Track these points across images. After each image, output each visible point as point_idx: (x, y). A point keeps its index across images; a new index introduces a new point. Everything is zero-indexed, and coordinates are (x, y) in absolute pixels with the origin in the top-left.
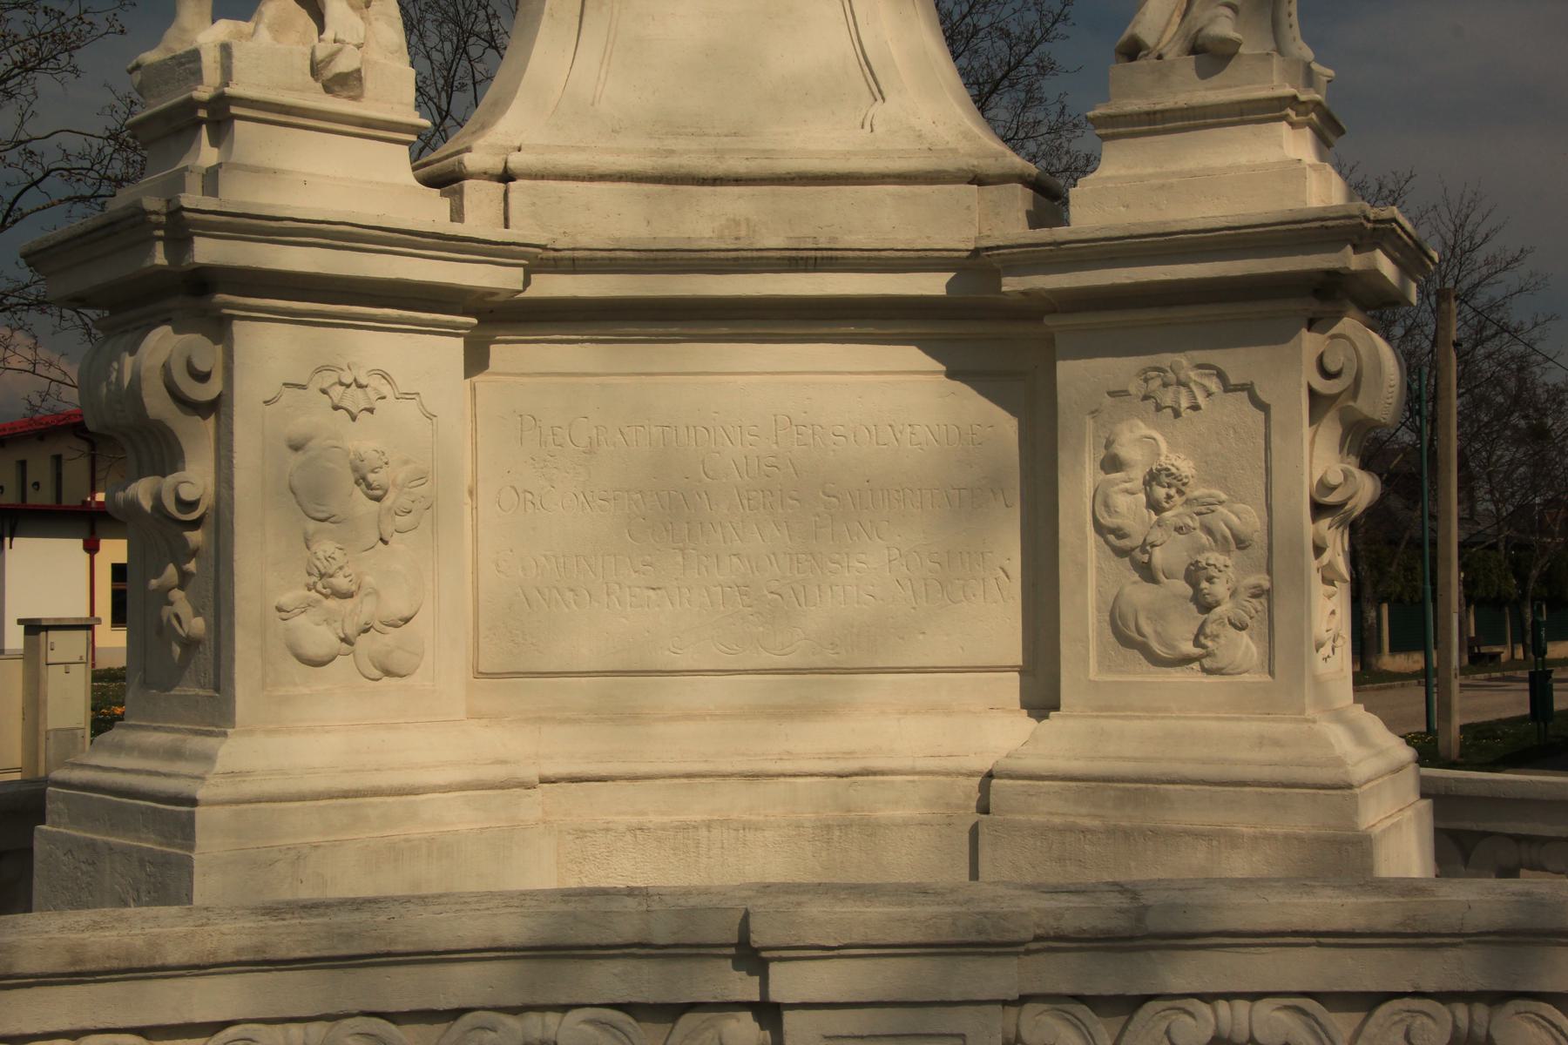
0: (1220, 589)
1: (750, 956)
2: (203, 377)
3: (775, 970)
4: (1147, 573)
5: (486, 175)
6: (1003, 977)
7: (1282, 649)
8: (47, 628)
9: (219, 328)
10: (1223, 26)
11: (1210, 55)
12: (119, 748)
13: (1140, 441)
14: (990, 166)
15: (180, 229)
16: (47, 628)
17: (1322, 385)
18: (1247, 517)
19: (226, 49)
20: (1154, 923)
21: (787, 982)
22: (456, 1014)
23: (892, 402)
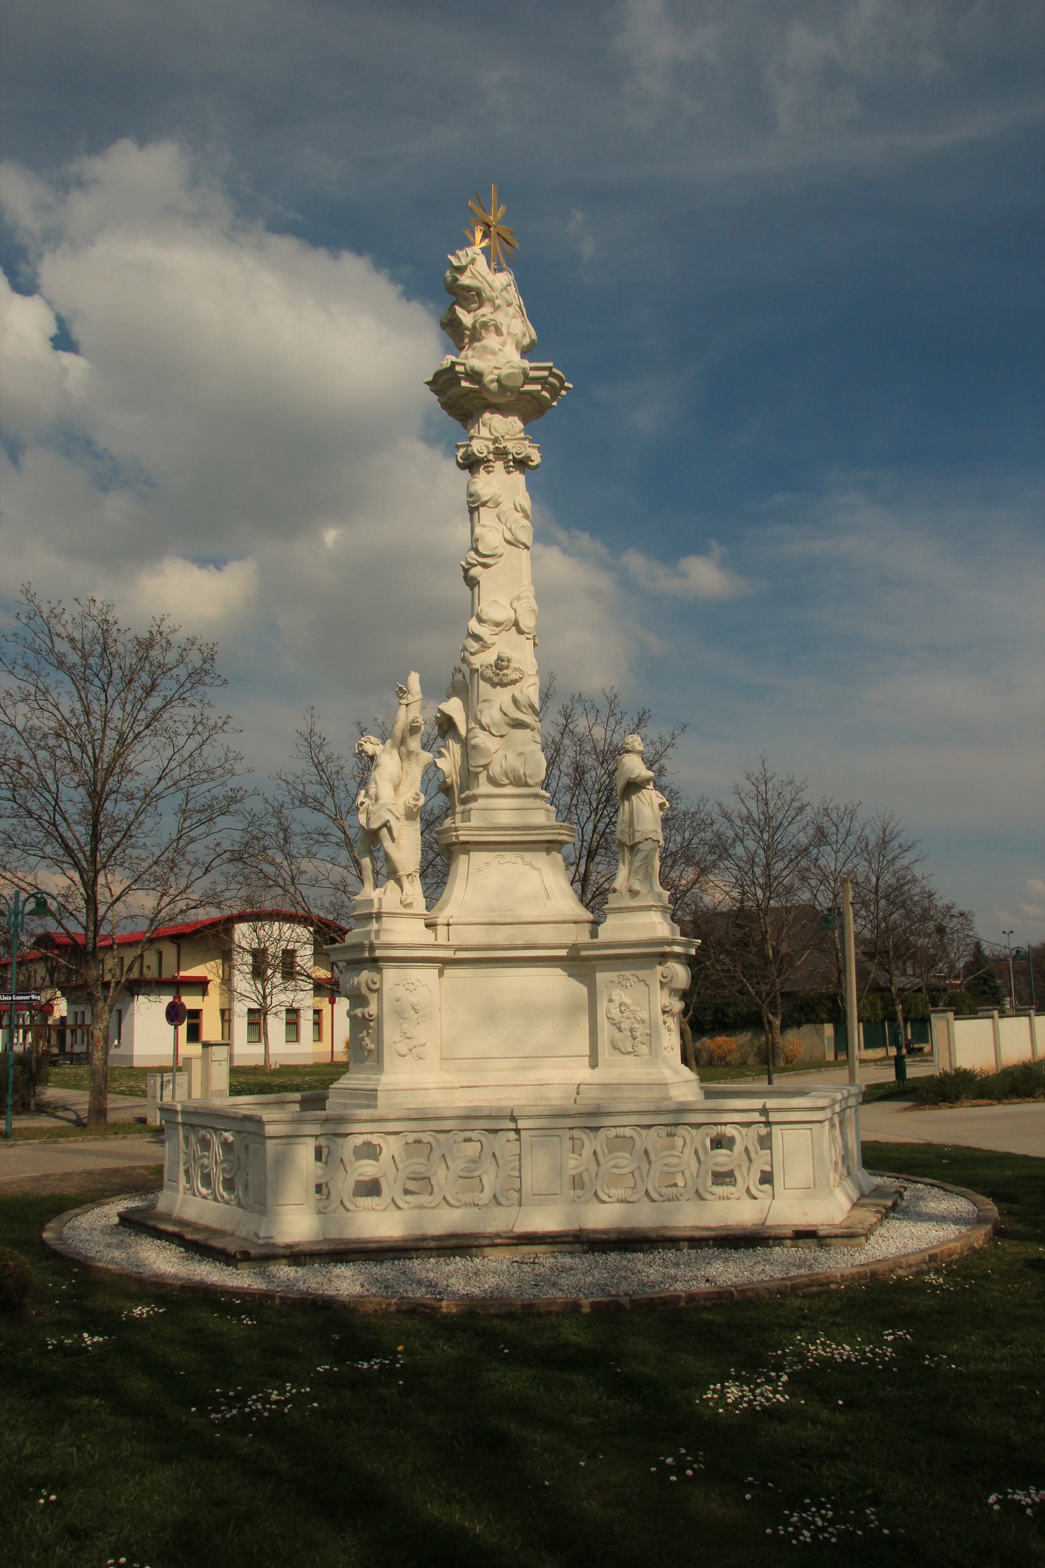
0: (638, 1034)
1: (513, 1118)
2: (375, 983)
4: (620, 1030)
5: (443, 924)
6: (569, 1122)
7: (654, 1052)
8: (212, 1045)
9: (379, 970)
10: (637, 886)
11: (633, 893)
12: (349, 1079)
14: (579, 919)
15: (372, 947)
16: (212, 1045)
17: (663, 980)
18: (644, 1015)
19: (380, 900)
20: (602, 1110)
21: (521, 1124)
22: (450, 1131)
23: (553, 985)
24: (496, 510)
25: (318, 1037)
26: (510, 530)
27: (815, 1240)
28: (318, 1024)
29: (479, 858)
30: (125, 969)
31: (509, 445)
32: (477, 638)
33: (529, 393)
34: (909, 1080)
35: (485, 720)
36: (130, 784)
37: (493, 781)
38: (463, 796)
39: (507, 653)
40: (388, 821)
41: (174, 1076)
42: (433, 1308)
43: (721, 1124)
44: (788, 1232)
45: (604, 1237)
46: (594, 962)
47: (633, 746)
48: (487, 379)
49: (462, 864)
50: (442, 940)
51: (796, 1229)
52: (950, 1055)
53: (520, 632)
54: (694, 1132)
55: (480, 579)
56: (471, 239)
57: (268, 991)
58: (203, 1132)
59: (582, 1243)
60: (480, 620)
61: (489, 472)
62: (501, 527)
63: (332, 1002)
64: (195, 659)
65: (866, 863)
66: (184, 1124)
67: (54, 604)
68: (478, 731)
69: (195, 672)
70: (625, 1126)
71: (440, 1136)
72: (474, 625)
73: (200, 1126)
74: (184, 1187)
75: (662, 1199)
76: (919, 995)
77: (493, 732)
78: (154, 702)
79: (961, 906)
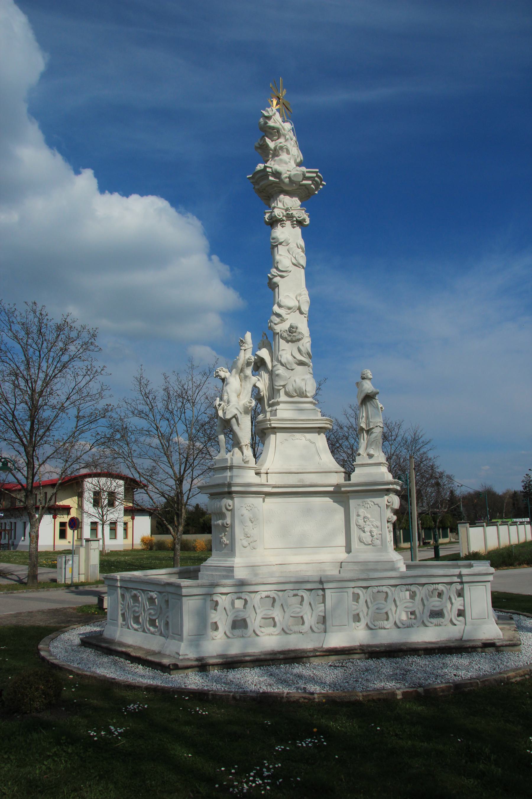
0: (374, 534)
2: (230, 506)
3: (324, 584)
4: (364, 531)
9: (232, 499)
13: (362, 511)
14: (338, 470)
15: (230, 485)
17: (388, 504)
22: (285, 590)
24: (287, 247)
25: (126, 537)
26: (295, 258)
27: (494, 648)
28: (125, 530)
29: (280, 436)
30: (48, 500)
31: (295, 213)
32: (278, 315)
33: (304, 185)
34: (40, 552)
35: (283, 361)
36: (53, 401)
37: (287, 394)
38: (270, 402)
39: (295, 323)
40: (236, 414)
41: (73, 557)
42: (309, 699)
43: (435, 583)
44: (479, 644)
45: (378, 649)
46: (348, 494)
47: (367, 376)
48: (284, 176)
49: (273, 439)
50: (264, 482)
51: (484, 641)
52: (468, 545)
53: (301, 313)
54: (420, 588)
55: (279, 284)
56: (271, 103)
57: (104, 513)
58: (135, 592)
59: (365, 653)
60: (280, 306)
61: (283, 227)
62: (290, 256)
63: (133, 519)
64: (85, 336)
65: (406, 451)
66: (121, 587)
67: (12, 306)
68: (279, 366)
69: (86, 344)
70: (383, 586)
71: (280, 593)
72: (276, 308)
73: (132, 588)
74: (121, 624)
75: (404, 626)
76: (427, 516)
77: (288, 367)
78: (65, 358)
79: (448, 472)
